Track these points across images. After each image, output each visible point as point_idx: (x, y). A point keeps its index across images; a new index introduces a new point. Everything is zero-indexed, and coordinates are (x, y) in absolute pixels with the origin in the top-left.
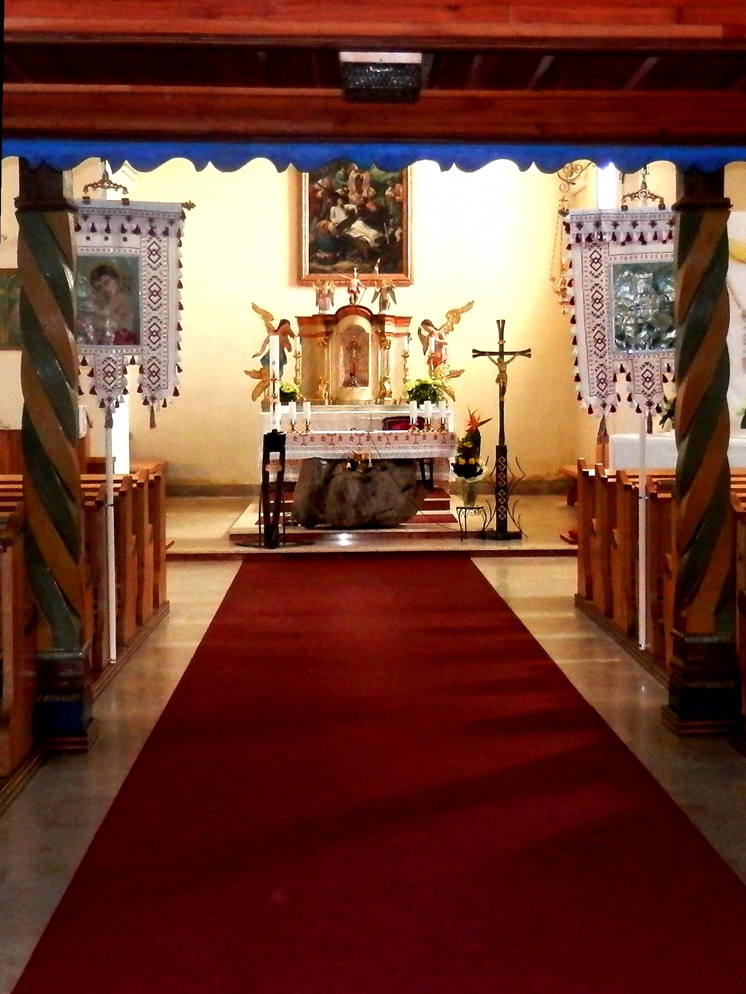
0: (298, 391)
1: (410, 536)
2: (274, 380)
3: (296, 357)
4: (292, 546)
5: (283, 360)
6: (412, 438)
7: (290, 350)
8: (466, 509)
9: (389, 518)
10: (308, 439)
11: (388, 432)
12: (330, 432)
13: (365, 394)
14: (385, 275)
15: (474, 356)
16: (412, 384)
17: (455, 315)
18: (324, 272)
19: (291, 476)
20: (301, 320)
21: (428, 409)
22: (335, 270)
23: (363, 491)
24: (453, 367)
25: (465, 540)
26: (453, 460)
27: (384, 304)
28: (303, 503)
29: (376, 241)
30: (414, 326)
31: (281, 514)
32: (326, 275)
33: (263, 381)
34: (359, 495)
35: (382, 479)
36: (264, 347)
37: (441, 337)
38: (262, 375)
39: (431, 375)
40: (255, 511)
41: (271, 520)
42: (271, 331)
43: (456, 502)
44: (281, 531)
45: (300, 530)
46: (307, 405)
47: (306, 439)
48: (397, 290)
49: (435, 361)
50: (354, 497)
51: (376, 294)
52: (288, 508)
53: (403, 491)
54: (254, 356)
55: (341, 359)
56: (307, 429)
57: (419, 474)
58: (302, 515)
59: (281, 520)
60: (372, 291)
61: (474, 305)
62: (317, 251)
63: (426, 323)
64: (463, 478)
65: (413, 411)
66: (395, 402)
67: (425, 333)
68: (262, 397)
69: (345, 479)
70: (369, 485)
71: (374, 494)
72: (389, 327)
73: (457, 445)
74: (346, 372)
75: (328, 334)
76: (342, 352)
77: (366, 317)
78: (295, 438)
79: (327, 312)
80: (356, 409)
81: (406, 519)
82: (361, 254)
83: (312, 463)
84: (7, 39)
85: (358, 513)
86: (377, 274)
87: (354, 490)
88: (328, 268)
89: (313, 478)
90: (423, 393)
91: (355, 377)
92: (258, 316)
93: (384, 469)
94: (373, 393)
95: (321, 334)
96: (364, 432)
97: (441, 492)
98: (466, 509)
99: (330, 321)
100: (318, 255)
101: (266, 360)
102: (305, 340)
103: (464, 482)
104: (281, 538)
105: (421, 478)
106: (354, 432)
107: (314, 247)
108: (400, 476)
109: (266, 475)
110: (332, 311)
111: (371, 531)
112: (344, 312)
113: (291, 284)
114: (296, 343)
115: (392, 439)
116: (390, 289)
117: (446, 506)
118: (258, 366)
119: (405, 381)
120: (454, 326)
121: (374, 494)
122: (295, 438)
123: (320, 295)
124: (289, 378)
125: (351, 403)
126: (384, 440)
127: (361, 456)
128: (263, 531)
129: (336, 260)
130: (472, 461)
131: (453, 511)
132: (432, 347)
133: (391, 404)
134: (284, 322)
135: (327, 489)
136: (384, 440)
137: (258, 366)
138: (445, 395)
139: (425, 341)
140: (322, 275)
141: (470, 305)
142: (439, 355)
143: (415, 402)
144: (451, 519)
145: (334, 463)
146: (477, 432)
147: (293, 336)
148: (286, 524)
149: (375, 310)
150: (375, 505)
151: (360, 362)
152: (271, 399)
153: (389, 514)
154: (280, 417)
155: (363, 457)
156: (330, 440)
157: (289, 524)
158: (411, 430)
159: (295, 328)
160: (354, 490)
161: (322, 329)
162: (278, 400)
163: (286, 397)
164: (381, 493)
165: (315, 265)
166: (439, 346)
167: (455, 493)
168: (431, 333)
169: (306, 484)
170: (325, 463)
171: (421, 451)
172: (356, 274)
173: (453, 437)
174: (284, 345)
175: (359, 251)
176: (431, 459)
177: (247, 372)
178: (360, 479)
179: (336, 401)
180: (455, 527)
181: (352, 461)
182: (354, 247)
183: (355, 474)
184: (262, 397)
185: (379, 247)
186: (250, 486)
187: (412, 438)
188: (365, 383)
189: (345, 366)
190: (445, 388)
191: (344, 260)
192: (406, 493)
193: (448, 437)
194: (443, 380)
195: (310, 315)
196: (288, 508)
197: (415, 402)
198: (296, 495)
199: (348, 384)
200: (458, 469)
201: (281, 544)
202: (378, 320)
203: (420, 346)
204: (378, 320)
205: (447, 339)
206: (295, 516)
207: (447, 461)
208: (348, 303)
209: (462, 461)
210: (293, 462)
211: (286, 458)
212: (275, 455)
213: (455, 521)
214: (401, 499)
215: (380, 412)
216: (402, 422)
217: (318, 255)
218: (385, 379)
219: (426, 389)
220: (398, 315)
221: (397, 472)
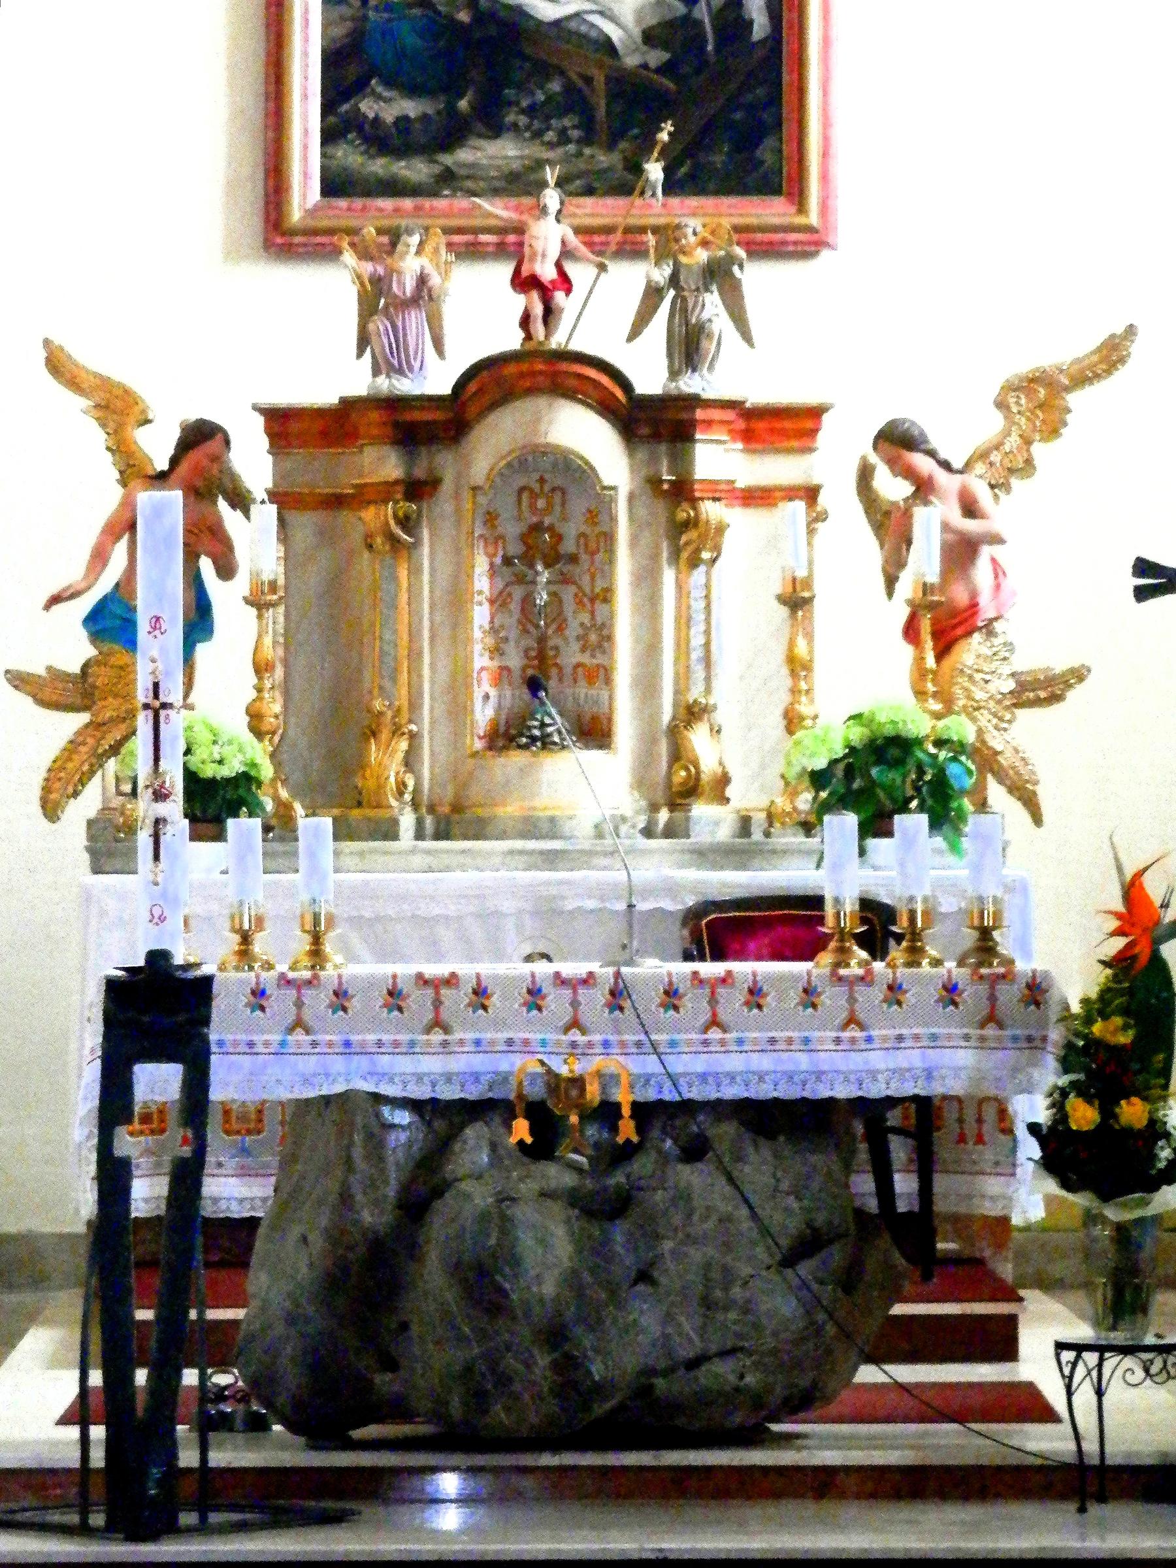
0: (267, 771)
1: (823, 1485)
2: (158, 710)
3: (257, 602)
4: (241, 1527)
5: (199, 619)
6: (832, 999)
7: (226, 570)
8: (1101, 1349)
9: (705, 1399)
10: (318, 1002)
11: (711, 969)
12: (433, 970)
13: (588, 786)
14: (693, 202)
15: (1141, 594)
16: (828, 740)
17: (1040, 400)
18: (393, 188)
19: (229, 1191)
20: (283, 425)
21: (907, 865)
22: (448, 179)
23: (595, 1253)
24: (1033, 657)
25: (1095, 1510)
26: (1032, 1108)
27: (688, 347)
28: (291, 1320)
29: (649, 37)
30: (836, 457)
31: (190, 1377)
32: (408, 203)
33: (94, 726)
34: (572, 1281)
35: (683, 1197)
36: (100, 557)
37: (970, 509)
38: (99, 696)
39: (920, 694)
40: (55, 1363)
41: (141, 1401)
42: (133, 470)
43: (1046, 1331)
44: (188, 1458)
45: (279, 1449)
46: (316, 828)
47: (311, 996)
48: (758, 278)
49: (944, 625)
50: (549, 1289)
51: (653, 294)
52: (218, 1346)
53: (789, 1260)
54: (55, 600)
55: (481, 615)
56: (317, 954)
57: (864, 1184)
58: (292, 1378)
59: (188, 1406)
60: (629, 279)
61: (1137, 349)
62: (360, 87)
63: (897, 440)
64: (1081, 1200)
65: (839, 868)
66: (745, 825)
67: (891, 487)
68: (89, 802)
69: (505, 1198)
70: (619, 1233)
71: (644, 1276)
72: (715, 458)
73: (1056, 1035)
74: (502, 675)
75: (418, 489)
76: (482, 583)
77: (606, 408)
78: (259, 993)
79: (406, 386)
80: (551, 859)
81: (803, 1402)
82: (575, 101)
83: (342, 1117)
84: (916, 1209)
85: (568, 1366)
86: (654, 206)
87: (547, 1252)
88: (416, 170)
89: (345, 1198)
90: (880, 780)
91: (549, 701)
92: (73, 408)
93: (695, 1150)
94: (641, 783)
95: (384, 492)
96: (594, 966)
97: (971, 1275)
98: (1101, 1349)
99: (425, 429)
100: (368, 107)
101: (112, 622)
102: (305, 523)
103: (1091, 1219)
104: (188, 1488)
105: (872, 1205)
106: (542, 968)
107: (345, 71)
108: (775, 1187)
109: (113, 1177)
110: (437, 378)
111: (631, 1459)
112: (494, 383)
113: (232, 253)
114: (255, 537)
115: (732, 1003)
116: (718, 274)
117: (999, 1341)
118: (71, 649)
119: (792, 722)
120: (1039, 450)
121: (644, 1276)
122: (259, 993)
123: (376, 299)
124: (221, 702)
125: (531, 828)
126: (695, 1006)
127: (578, 1082)
128: (98, 1458)
129: (451, 133)
130: (1132, 1112)
131: (1035, 1364)
132: (925, 561)
133: (724, 833)
134: (200, 436)
135: (414, 1251)
136: (695, 1006)
137: (71, 649)
138: (996, 793)
139: (892, 527)
140: (386, 203)
141: (1112, 355)
142: (961, 596)
143: (850, 820)
144: (1028, 1405)
145: (445, 1118)
146: (1158, 965)
147: (241, 501)
148: (210, 1425)
149: (649, 373)
150: (639, 1337)
151: (573, 629)
152: (144, 808)
153: (723, 1371)
154: (201, 900)
155: (593, 1093)
156: (429, 1003)
157: (223, 1423)
158: (826, 958)
159: (252, 460)
160: (547, 1252)
161: (384, 464)
162: (174, 809)
163: (213, 803)
164: (681, 1265)
165: (350, 156)
166: (961, 552)
167: (1049, 1285)
168: (923, 489)
169: (314, 1223)
170: (403, 1117)
171: (877, 1060)
172: (552, 198)
173: (1036, 991)
174: (206, 541)
175: (569, 89)
176: (923, 1104)
177: (19, 680)
178: (573, 1198)
179: (452, 819)
180: (1044, 1441)
181: (537, 1112)
182: (544, 70)
183: (554, 1175)
184: (89, 802)
185: (665, 69)
186: (26, 1239)
187: (832, 999)
188: (594, 732)
189: (497, 651)
190: (987, 760)
191: (496, 130)
192: (805, 1268)
193: (1009, 995)
194: (984, 718)
195: (328, 397)
196: (218, 1346)
197: (850, 820)
198: (258, 1280)
199: (513, 735)
200: (1063, 1153)
201: (187, 1518)
202: (658, 424)
203: (869, 551)
204: (658, 424)
205: (1000, 514)
206: (260, 1385)
207: (1003, 1114)
208: (512, 340)
209: (1083, 1115)
210: (249, 1121)
211: (217, 1094)
212: (157, 1082)
213: (1047, 1414)
214: (779, 1304)
215: (675, 878)
216: (789, 925)
217: (368, 107)
218: (692, 713)
219: (898, 763)
220: (756, 397)
221: (759, 1167)
